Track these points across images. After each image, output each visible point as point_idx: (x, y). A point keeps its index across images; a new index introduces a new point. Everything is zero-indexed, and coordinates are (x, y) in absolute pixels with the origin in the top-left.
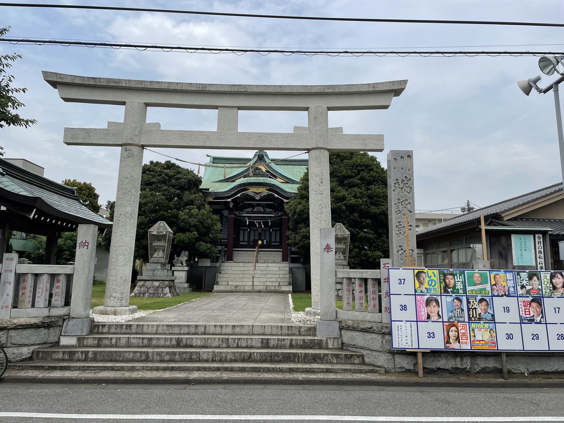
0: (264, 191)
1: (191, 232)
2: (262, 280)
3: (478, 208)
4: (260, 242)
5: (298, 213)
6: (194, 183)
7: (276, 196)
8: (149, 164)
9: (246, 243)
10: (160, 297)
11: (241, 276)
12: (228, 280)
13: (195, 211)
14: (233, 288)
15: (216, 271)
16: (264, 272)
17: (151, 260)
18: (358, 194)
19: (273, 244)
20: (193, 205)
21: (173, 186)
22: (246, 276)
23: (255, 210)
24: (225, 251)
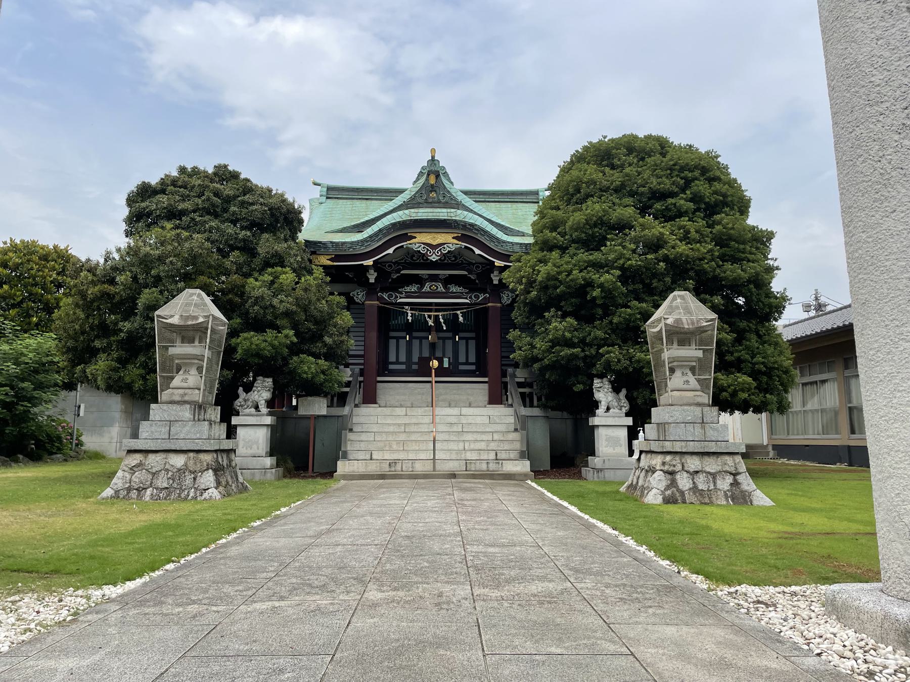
0: (448, 241)
1: (278, 329)
2: (453, 446)
3: (839, 306)
5: (541, 282)
6: (286, 219)
7: (477, 252)
8: (175, 174)
9: (403, 367)
10: (186, 499)
11: (403, 437)
12: (371, 447)
13: (287, 277)
14: (385, 468)
15: (343, 426)
16: (455, 429)
17: (164, 396)
18: (693, 234)
19: (462, 367)
20: (283, 266)
21: (234, 222)
22: (413, 437)
23: (426, 288)
24: (360, 382)
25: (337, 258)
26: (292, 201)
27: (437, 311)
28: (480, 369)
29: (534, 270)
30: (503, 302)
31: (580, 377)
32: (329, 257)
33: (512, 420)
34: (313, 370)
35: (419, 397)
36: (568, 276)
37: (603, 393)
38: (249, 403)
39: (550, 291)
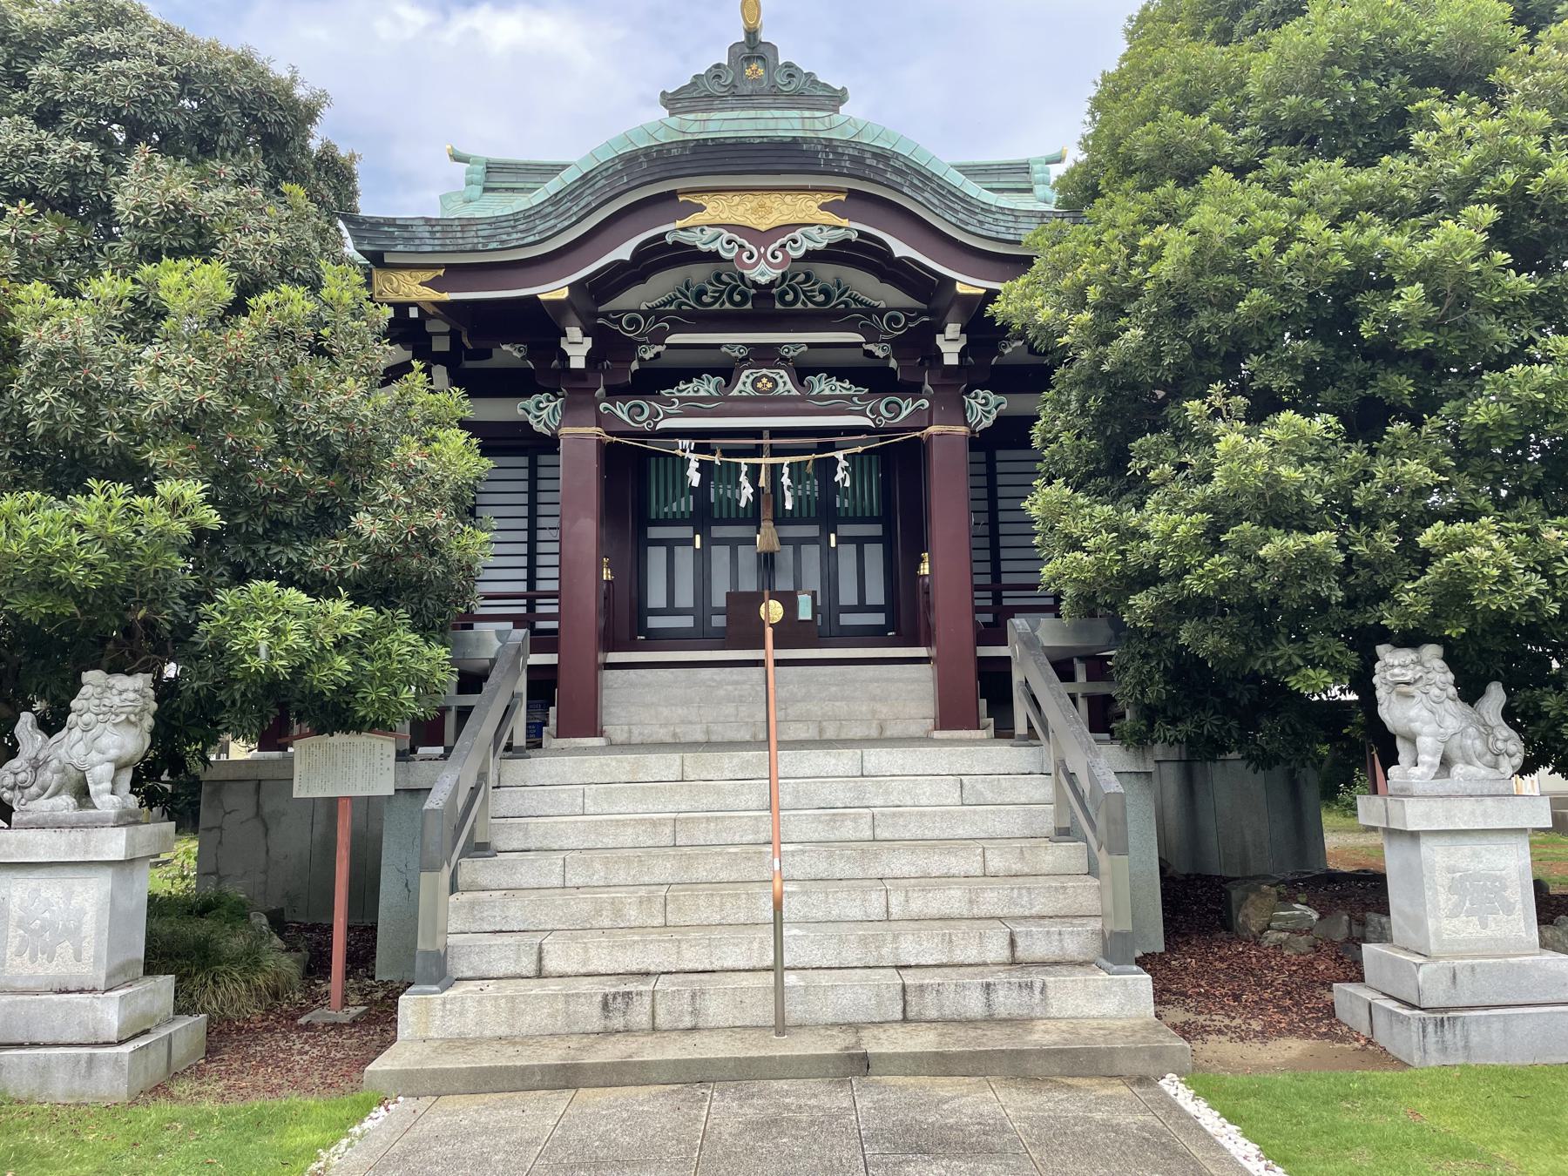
1: (139, 477)
4: (774, 611)
9: (687, 622)
11: (664, 870)
19: (847, 619)
23: (744, 385)
25: (456, 274)
26: (286, 75)
27: (775, 452)
28: (904, 620)
29: (1134, 249)
30: (972, 420)
31: (1316, 640)
32: (428, 275)
33: (1041, 789)
34: (294, 639)
35: (729, 709)
36: (1280, 249)
37: (1415, 693)
38: (49, 776)
39: (1204, 319)
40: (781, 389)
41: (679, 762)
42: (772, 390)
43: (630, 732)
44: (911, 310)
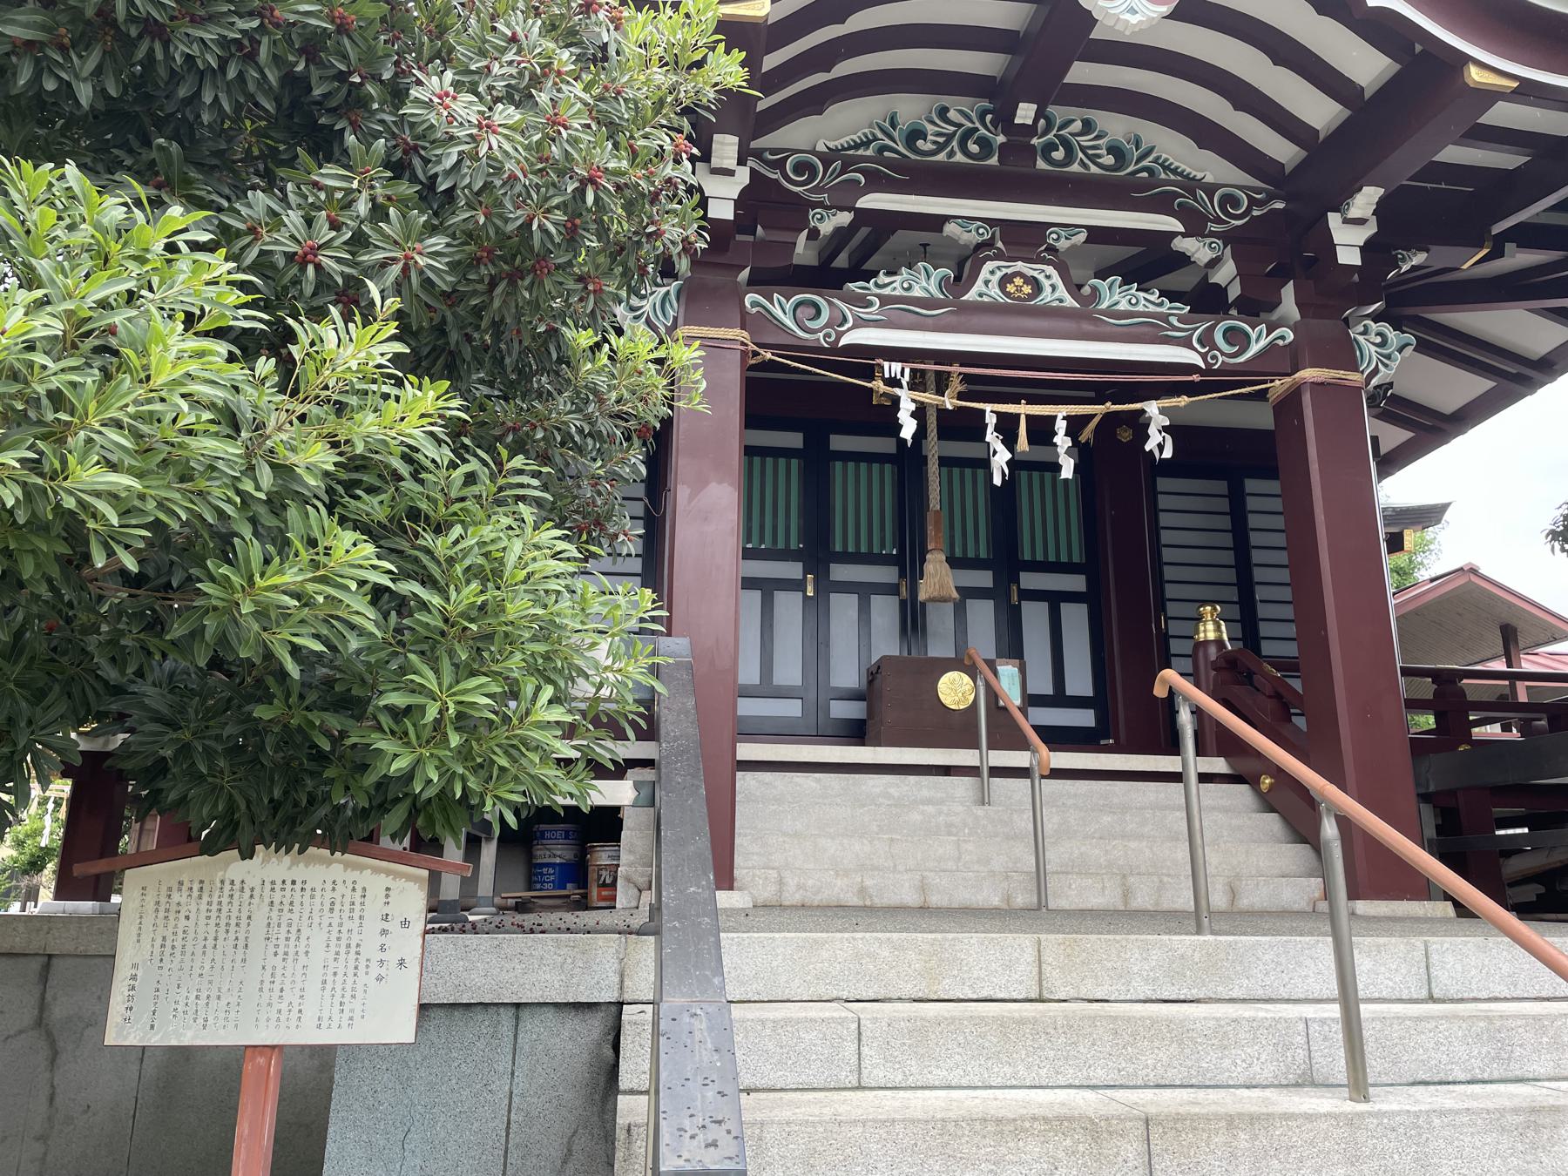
23: (986, 285)
40: (1047, 296)
41: (1029, 955)
42: (1032, 297)
43: (781, 882)
44: (1258, 191)
